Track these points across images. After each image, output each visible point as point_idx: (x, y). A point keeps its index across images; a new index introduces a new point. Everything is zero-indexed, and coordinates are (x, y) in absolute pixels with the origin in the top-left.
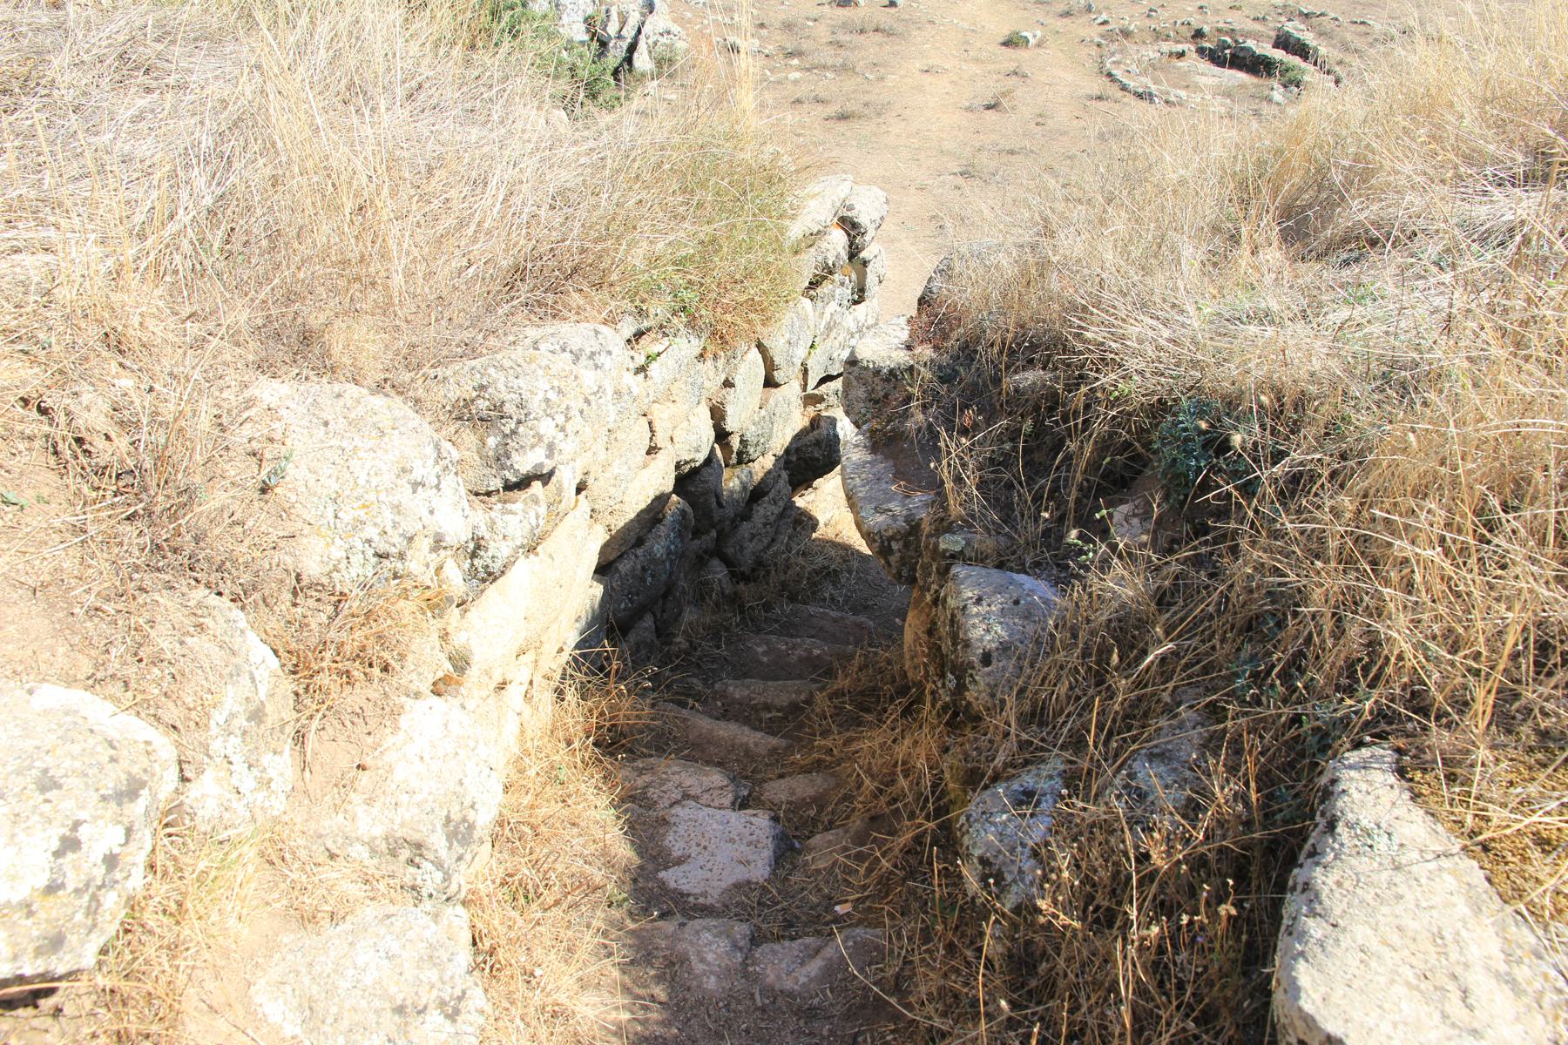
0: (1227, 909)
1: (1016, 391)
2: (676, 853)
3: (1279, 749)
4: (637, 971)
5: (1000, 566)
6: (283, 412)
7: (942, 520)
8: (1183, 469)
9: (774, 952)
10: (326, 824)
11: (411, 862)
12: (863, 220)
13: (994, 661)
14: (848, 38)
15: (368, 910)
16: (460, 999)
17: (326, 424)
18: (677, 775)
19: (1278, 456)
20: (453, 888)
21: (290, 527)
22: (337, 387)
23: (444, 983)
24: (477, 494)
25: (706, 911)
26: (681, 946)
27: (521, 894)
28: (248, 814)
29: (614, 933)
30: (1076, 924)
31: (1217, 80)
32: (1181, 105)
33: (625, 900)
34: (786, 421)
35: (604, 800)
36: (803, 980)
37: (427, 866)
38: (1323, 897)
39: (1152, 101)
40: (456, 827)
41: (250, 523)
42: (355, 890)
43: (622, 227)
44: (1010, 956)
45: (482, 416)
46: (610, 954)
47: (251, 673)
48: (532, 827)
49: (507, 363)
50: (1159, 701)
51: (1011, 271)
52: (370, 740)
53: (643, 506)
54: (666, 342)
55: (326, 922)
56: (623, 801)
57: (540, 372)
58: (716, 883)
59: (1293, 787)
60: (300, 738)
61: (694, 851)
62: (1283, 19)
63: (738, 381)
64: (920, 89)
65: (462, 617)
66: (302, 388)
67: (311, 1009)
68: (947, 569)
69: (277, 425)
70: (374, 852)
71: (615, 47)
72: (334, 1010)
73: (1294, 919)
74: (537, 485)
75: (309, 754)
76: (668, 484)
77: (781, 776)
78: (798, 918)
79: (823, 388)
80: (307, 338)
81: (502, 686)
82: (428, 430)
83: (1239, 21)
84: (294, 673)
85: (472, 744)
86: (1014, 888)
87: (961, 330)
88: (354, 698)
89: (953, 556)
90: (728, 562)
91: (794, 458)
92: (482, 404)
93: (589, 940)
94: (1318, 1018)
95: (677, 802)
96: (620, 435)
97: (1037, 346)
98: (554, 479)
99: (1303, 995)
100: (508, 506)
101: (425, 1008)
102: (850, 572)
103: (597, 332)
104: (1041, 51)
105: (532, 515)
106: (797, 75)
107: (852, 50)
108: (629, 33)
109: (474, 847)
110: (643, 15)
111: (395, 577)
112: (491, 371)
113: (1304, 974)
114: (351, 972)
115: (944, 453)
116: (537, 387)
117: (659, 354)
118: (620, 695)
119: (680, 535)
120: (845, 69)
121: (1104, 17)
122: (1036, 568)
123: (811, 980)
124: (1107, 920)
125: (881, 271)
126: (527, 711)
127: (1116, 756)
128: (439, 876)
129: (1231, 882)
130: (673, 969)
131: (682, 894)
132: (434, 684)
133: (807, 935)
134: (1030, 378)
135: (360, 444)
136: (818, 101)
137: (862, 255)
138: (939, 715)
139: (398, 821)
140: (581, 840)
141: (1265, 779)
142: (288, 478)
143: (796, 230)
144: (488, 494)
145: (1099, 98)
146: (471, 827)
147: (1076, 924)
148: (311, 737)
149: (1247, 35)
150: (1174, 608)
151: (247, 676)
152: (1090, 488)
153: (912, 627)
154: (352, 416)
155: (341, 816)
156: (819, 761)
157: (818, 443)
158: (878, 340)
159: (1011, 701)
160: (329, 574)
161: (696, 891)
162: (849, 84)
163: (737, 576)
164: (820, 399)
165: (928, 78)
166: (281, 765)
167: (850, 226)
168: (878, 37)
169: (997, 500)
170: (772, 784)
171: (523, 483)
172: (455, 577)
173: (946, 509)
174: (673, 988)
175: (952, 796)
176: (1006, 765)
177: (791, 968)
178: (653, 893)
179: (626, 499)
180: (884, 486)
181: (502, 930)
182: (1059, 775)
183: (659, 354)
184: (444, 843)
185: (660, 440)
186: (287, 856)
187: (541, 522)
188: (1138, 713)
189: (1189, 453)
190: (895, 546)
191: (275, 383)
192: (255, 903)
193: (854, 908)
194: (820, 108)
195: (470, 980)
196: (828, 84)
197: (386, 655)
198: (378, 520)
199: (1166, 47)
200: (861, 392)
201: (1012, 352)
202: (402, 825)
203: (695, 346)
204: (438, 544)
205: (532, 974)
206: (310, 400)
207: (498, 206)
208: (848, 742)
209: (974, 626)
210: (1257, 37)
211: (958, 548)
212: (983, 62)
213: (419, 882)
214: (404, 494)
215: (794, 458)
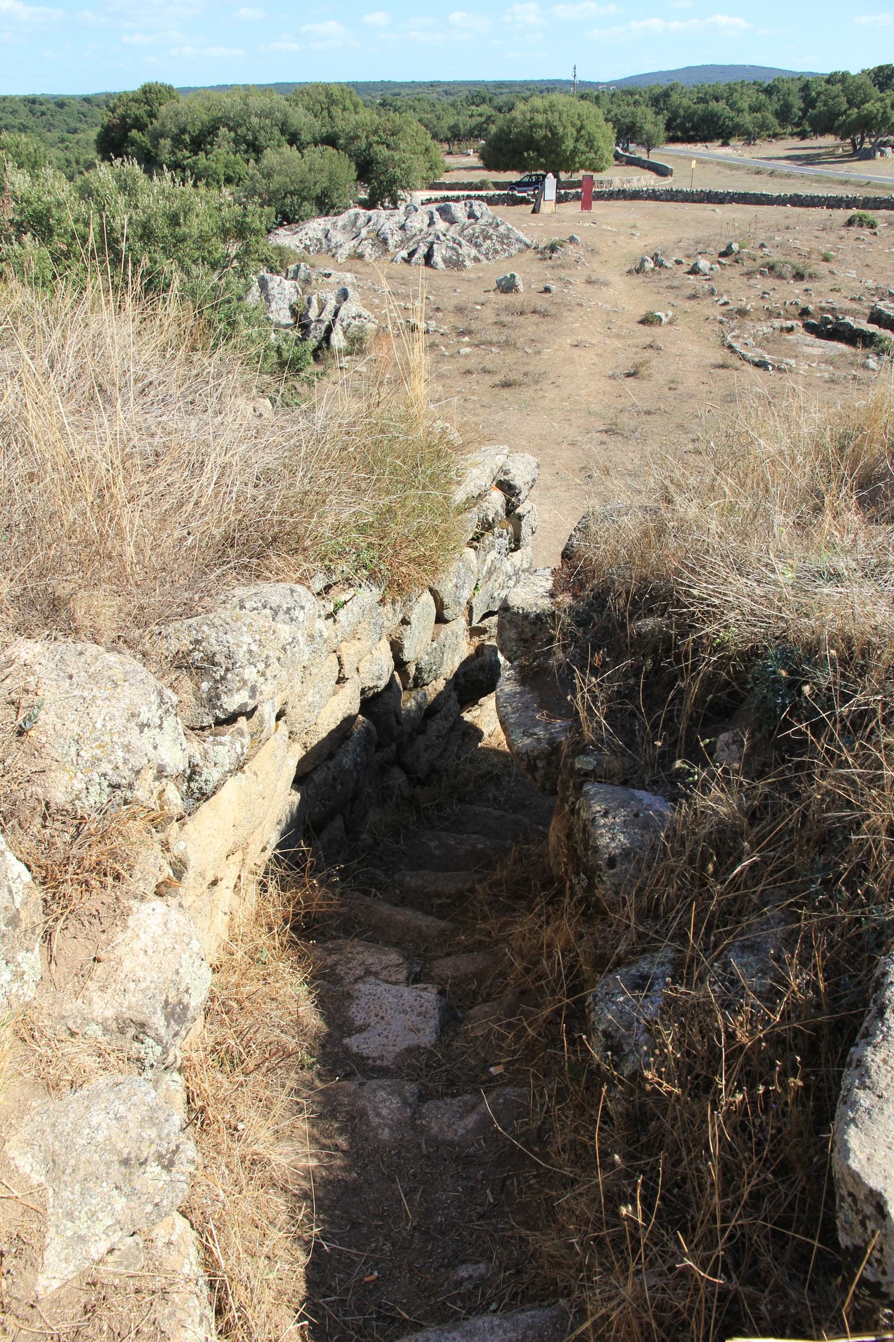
0: (796, 1082)
1: (639, 634)
2: (358, 1022)
3: (843, 945)
4: (324, 1124)
5: (625, 783)
6: (37, 668)
7: (578, 743)
8: (771, 705)
9: (438, 1108)
10: (68, 1007)
11: (136, 1038)
12: (518, 482)
13: (618, 865)
14: (509, 319)
15: (101, 1079)
16: (174, 1152)
17: (71, 677)
18: (362, 955)
19: (845, 698)
20: (171, 1059)
21: (41, 764)
22: (80, 646)
23: (161, 1139)
24: (193, 729)
25: (383, 1072)
26: (360, 1103)
27: (226, 1059)
28: (6, 1001)
29: (305, 1092)
30: (677, 1091)
31: (821, 350)
32: (791, 371)
33: (314, 1063)
34: (454, 650)
35: (298, 978)
36: (461, 1131)
37: (149, 1041)
38: (872, 1072)
39: (767, 369)
40: (174, 1009)
41: (9, 761)
42: (90, 1062)
43: (309, 503)
44: (628, 1115)
45: (198, 666)
46: (301, 1111)
47: (9, 887)
48: (238, 1002)
49: (217, 622)
50: (750, 901)
51: (635, 534)
52: (104, 937)
53: (333, 726)
54: (352, 591)
55: (66, 1090)
56: (314, 977)
57: (245, 629)
58: (391, 1048)
59: (856, 976)
60: (48, 936)
61: (373, 1020)
62: (876, 299)
63: (413, 619)
64: (571, 361)
65: (181, 829)
66: (52, 647)
67: (54, 1161)
68: (581, 785)
69: (31, 679)
70: (106, 1030)
71: (315, 328)
72: (72, 1162)
73: (849, 1090)
74: (242, 720)
75: (54, 950)
76: (354, 707)
77: (448, 955)
78: (459, 1078)
79: (486, 622)
80: (56, 605)
81: (214, 883)
82: (152, 679)
83: (838, 301)
84: (44, 884)
85: (186, 940)
86: (631, 1058)
87: (595, 582)
88: (91, 903)
89: (587, 774)
90: (406, 770)
91: (462, 681)
92: (197, 655)
93: (282, 1099)
94: (862, 1175)
95: (361, 978)
96: (314, 671)
97: (656, 597)
98: (257, 713)
99: (852, 1155)
100: (218, 738)
101: (146, 1160)
102: (510, 776)
103: (292, 591)
104: (672, 328)
105: (238, 746)
106: (468, 350)
107: (514, 329)
108: (327, 316)
109: (188, 1024)
110: (338, 302)
111: (126, 802)
112: (205, 628)
113: (854, 1138)
114: (87, 1131)
115: (578, 689)
116: (243, 642)
117: (345, 603)
118: (312, 887)
119: (365, 749)
120: (507, 344)
121: (725, 298)
122: (653, 786)
123: (468, 1132)
124: (701, 1088)
125: (534, 524)
126: (236, 900)
127: (716, 946)
128: (158, 1049)
129: (798, 1058)
130: (354, 1122)
131: (362, 1058)
132: (158, 886)
133: (466, 1092)
134: (649, 623)
135: (98, 694)
136: (485, 371)
137: (518, 511)
138: (576, 907)
139: (126, 1004)
140: (279, 1013)
141: (832, 970)
142: (40, 723)
143: (459, 496)
144: (203, 729)
145: (722, 367)
146: (186, 1008)
147: (677, 1091)
148: (57, 935)
149: (846, 312)
150: (764, 823)
151: (6, 890)
152: (698, 717)
153: (555, 831)
154: (92, 670)
155: (80, 1001)
156: (480, 942)
157: (482, 668)
158: (528, 589)
159: (631, 899)
160: (72, 802)
161: (375, 1055)
162: (511, 357)
163: (415, 781)
164: (483, 631)
165: (577, 352)
166: (32, 960)
167: (507, 487)
168: (535, 318)
169: (623, 726)
170: (441, 961)
171: (232, 719)
172: (174, 795)
173: (581, 734)
174: (353, 1138)
175: (586, 976)
176: (627, 953)
177: (450, 1121)
178: (337, 1057)
179: (319, 721)
180: (531, 713)
181: (211, 1091)
182: (670, 962)
183: (345, 603)
184: (163, 1022)
185: (348, 671)
186: (36, 1034)
187: (245, 751)
188: (732, 912)
189: (776, 693)
190: (540, 764)
191: (30, 643)
192: (9, 1074)
193: (506, 1070)
194: (487, 377)
195: (183, 1137)
196: (494, 357)
197: (117, 866)
198: (112, 758)
199: (777, 323)
200: (512, 634)
201: (634, 603)
202: (129, 1008)
203: (376, 593)
204: (161, 773)
205: (236, 1129)
206: (58, 657)
207: (212, 486)
208: (503, 926)
209: (601, 835)
210: (854, 314)
211: (590, 768)
212: (624, 338)
213: (142, 1055)
214: (133, 735)
215: (462, 681)
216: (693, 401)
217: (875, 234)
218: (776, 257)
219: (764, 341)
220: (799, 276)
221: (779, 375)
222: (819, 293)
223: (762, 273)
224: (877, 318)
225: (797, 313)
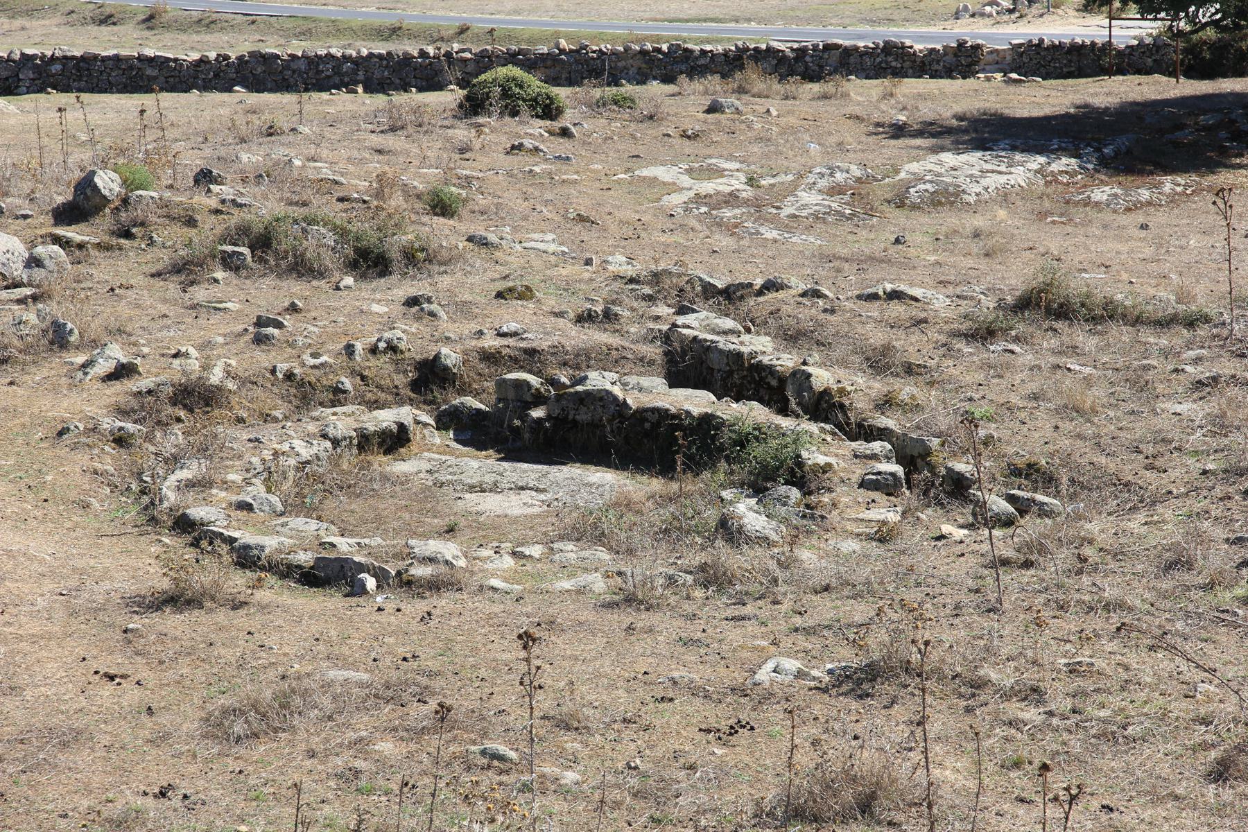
121: (116, 353)
145: (176, 600)
149: (581, 360)
199: (343, 421)
210: (610, 359)
216: (81, 757)
217: (565, 133)
218: (265, 207)
219: (308, 491)
220: (370, 262)
221: (415, 607)
222: (463, 309)
223: (229, 262)
224: (690, 364)
225: (400, 380)
